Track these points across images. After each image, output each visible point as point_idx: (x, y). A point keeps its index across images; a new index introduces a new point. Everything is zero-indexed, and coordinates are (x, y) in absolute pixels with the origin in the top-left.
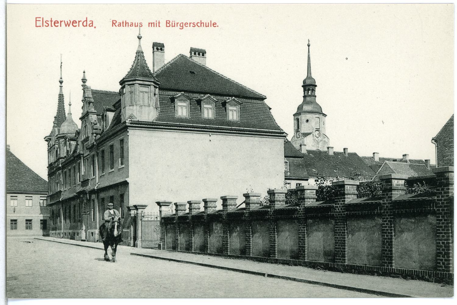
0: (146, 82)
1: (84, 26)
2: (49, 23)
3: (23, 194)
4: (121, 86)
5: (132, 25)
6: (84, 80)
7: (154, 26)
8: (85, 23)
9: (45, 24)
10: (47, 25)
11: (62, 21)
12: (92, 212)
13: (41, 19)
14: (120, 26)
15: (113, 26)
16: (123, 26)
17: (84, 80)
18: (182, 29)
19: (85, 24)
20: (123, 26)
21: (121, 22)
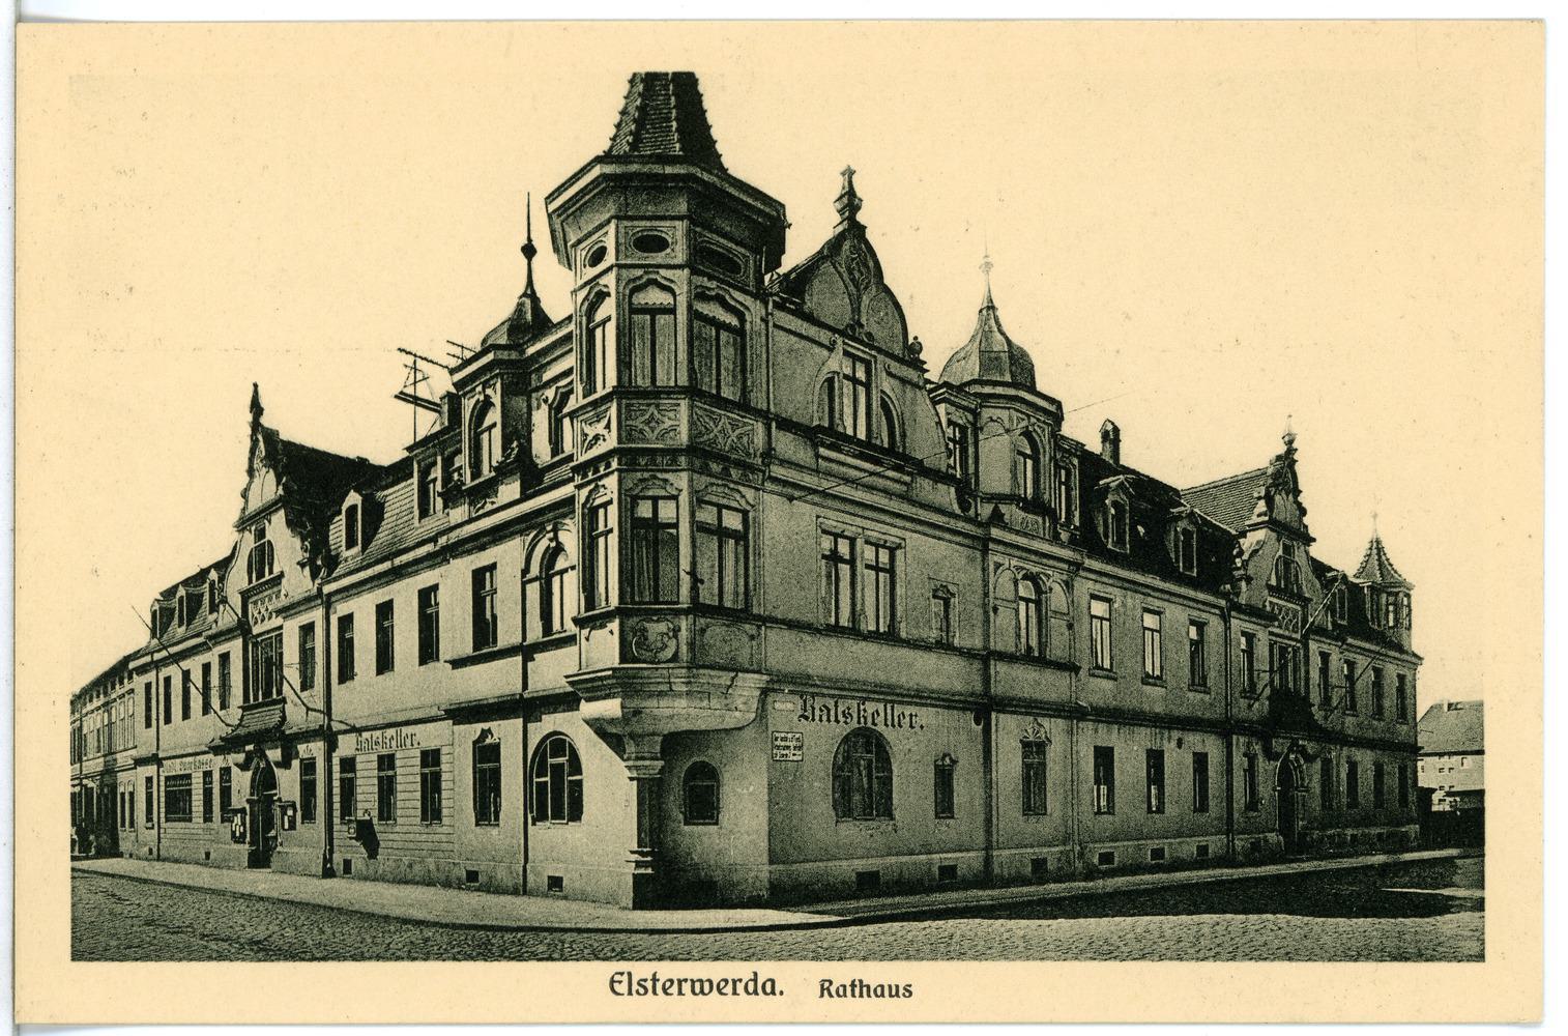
0: (849, 601)
1: (748, 993)
2: (649, 985)
3: (525, 784)
4: (141, 638)
5: (668, 984)
6: (256, 408)
7: (890, 986)
8: (751, 985)
9: (635, 987)
10: (642, 991)
11: (686, 980)
12: (1154, 803)
13: (625, 978)
14: (883, 995)
15: (822, 995)
16: (853, 995)
17: (256, 408)
18: (642, 980)
19: (751, 988)
20: (853, 995)
21: (848, 983)
